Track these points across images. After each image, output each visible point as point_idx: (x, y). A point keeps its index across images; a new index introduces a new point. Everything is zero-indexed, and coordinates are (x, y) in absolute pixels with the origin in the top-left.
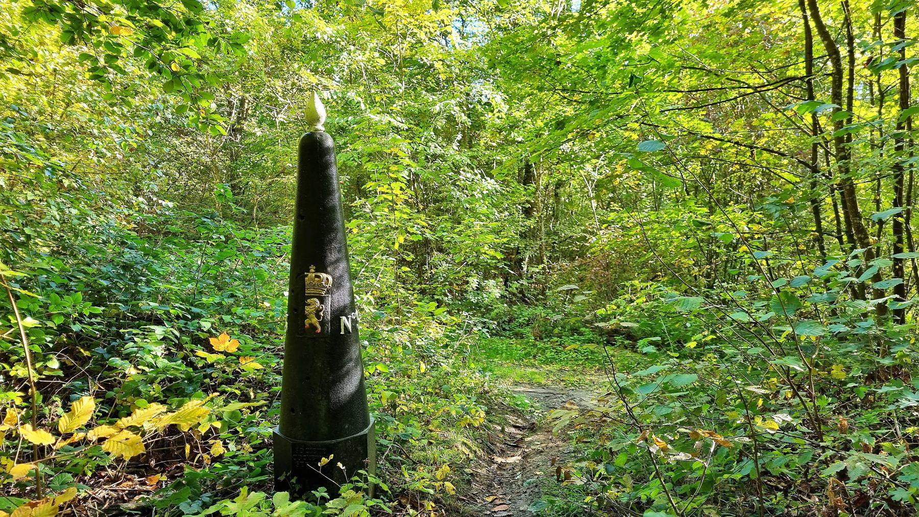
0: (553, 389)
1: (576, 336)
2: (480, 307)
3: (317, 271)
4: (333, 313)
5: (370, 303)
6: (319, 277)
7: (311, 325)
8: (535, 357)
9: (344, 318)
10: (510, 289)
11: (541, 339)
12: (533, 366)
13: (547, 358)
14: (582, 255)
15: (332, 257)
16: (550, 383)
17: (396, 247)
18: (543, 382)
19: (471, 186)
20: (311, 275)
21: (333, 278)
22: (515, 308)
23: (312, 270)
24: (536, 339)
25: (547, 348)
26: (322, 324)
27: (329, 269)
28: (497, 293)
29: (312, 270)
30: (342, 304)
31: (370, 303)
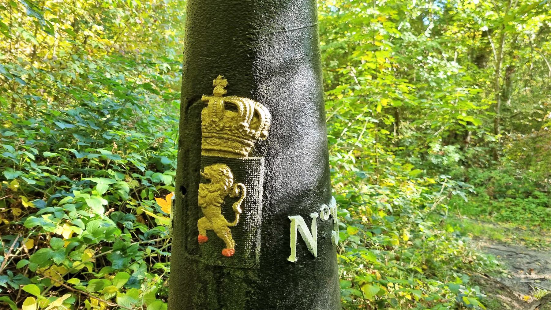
0: (514, 248)
1: (530, 198)
2: (440, 168)
3: (231, 91)
4: (268, 206)
5: (351, 162)
6: (233, 107)
7: (211, 233)
8: (490, 214)
9: (297, 221)
10: (466, 154)
11: (495, 198)
12: (490, 222)
13: (502, 216)
14: (538, 126)
15: (273, 54)
16: (510, 241)
17: (379, 109)
18: (504, 239)
19: (437, 68)
20: (215, 102)
21: (274, 114)
22: (470, 170)
23: (219, 89)
24: (490, 198)
25: (501, 207)
26: (239, 233)
27: (263, 88)
28: (457, 157)
29: (219, 89)
30: (296, 185)
31: (351, 162)
